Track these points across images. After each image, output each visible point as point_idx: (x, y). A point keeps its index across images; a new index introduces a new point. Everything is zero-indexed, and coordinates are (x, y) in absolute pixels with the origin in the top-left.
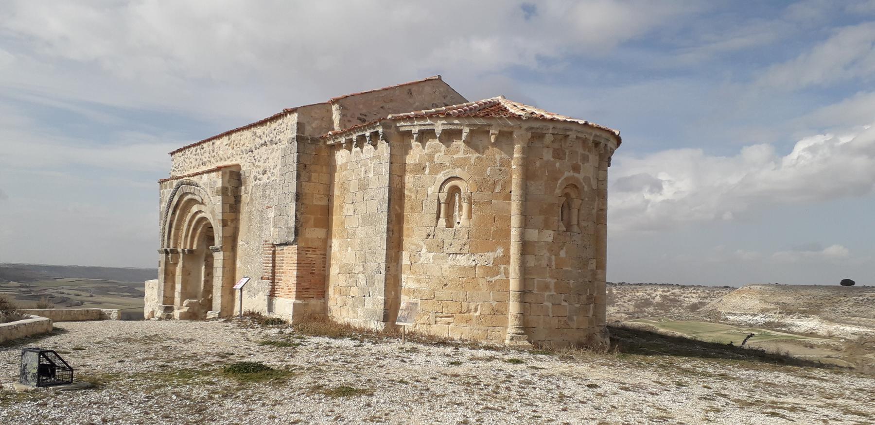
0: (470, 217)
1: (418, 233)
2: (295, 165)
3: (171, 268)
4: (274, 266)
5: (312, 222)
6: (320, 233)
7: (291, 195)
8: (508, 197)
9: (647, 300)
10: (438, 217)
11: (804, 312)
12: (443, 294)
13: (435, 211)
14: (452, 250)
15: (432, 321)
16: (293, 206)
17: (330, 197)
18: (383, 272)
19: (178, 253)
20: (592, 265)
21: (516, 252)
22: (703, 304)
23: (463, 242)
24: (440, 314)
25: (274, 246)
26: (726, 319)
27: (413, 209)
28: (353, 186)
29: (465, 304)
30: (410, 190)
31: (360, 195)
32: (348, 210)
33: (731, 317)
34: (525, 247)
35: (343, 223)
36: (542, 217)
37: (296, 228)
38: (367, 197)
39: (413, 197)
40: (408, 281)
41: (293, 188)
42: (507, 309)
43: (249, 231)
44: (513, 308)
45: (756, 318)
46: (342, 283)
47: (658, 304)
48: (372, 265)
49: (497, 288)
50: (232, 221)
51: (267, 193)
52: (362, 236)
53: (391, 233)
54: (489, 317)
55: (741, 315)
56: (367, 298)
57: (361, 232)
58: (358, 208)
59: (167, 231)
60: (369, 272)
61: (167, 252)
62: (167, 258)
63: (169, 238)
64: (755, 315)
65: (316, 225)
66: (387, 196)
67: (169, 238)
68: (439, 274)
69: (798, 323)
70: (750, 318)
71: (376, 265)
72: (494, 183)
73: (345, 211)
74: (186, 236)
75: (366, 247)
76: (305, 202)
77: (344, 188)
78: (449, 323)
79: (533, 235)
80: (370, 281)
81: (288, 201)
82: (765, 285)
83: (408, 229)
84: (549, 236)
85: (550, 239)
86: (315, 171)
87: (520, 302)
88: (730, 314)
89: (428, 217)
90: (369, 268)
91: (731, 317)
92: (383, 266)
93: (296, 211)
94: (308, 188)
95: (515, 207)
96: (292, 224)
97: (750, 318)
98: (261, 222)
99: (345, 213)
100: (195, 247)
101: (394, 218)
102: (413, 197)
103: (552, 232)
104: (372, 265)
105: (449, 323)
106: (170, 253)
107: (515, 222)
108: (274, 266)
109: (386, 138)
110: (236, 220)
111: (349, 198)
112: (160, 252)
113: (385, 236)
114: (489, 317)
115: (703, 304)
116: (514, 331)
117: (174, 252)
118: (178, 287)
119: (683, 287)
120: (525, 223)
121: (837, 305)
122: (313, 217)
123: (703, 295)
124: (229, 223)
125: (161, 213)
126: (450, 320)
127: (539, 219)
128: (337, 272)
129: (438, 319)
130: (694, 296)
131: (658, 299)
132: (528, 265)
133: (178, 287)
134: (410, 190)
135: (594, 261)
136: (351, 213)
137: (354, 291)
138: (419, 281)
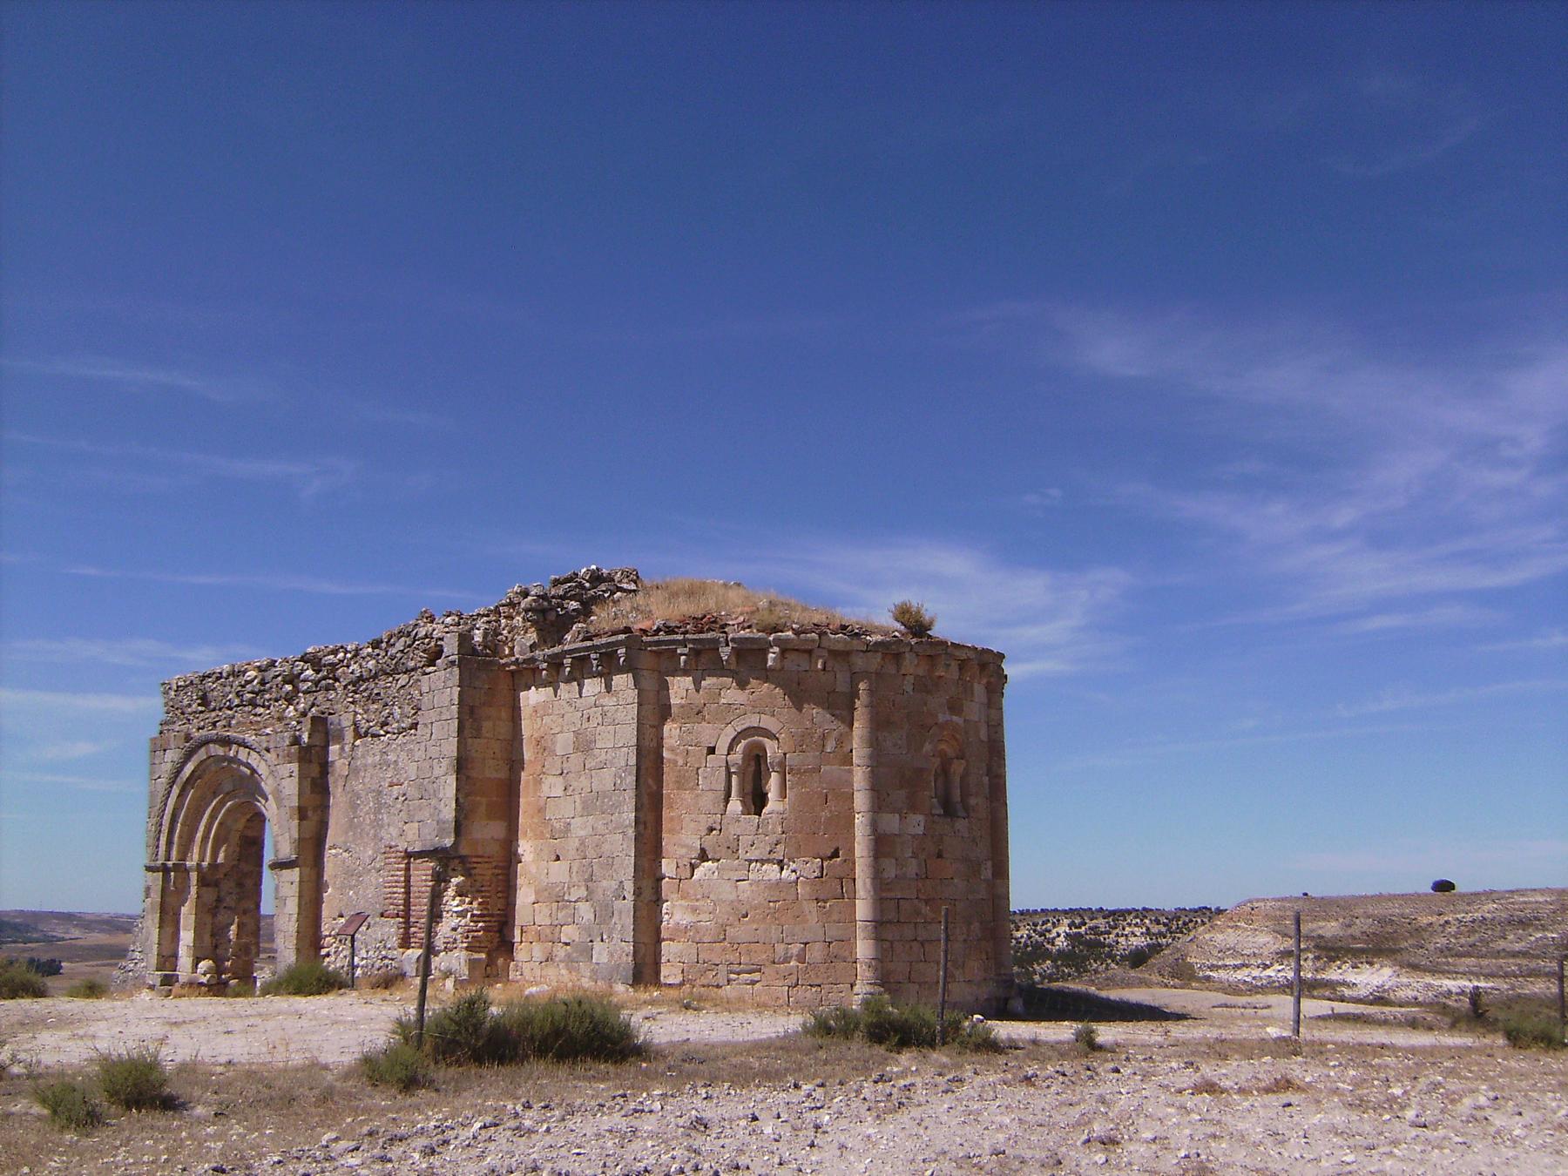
0: (783, 795)
1: (693, 825)
2: (455, 708)
3: (170, 900)
4: (408, 893)
5: (483, 809)
6: (496, 830)
7: (445, 763)
8: (847, 760)
9: (1038, 946)
10: (727, 800)
11: (1363, 951)
12: (738, 932)
13: (722, 786)
14: (754, 854)
15: (722, 981)
16: (452, 780)
17: (515, 764)
18: (630, 897)
19: (187, 871)
20: (987, 873)
21: (865, 853)
22: (1156, 949)
23: (773, 838)
24: (736, 968)
25: (409, 855)
26: (1208, 978)
27: (680, 785)
28: (563, 743)
29: (780, 948)
30: (672, 750)
31: (577, 759)
32: (553, 786)
33: (1221, 974)
34: (881, 845)
35: (541, 810)
36: (903, 793)
37: (457, 821)
38: (591, 763)
39: (680, 762)
40: (674, 913)
41: (451, 748)
42: (852, 950)
43: (351, 825)
44: (864, 949)
45: (1269, 972)
46: (543, 918)
47: (1061, 953)
48: (607, 885)
49: (835, 917)
50: (315, 810)
51: (392, 757)
52: (582, 833)
53: (641, 827)
54: (823, 968)
55: (1236, 967)
56: (597, 945)
57: (580, 828)
58: (575, 784)
59: (165, 829)
60: (599, 895)
61: (165, 870)
62: (166, 879)
63: (169, 843)
64: (1266, 967)
65: (491, 816)
66: (633, 761)
67: (191, 839)
68: (733, 897)
69: (1351, 976)
70: (1256, 973)
71: (614, 884)
72: (824, 737)
73: (545, 787)
74: (205, 838)
75: (591, 853)
76: (474, 774)
77: (542, 745)
78: (753, 983)
79: (891, 822)
80: (604, 914)
81: (438, 771)
82: (1283, 899)
83: (672, 819)
84: (916, 824)
85: (920, 830)
86: (489, 718)
87: (876, 939)
88: (1213, 967)
89: (709, 801)
90: (600, 891)
91: (1221, 974)
92: (629, 886)
93: (458, 790)
94: (475, 745)
95: (860, 778)
96: (449, 812)
97: (1256, 973)
98: (377, 811)
99: (545, 790)
100: (220, 860)
101: (645, 800)
102: (680, 762)
103: (921, 818)
104: (607, 885)
105: (753, 983)
106: (170, 875)
107: (861, 801)
108: (408, 893)
109: (630, 667)
110: (324, 808)
111: (553, 765)
112: (149, 869)
113: (631, 832)
114: (823, 968)
115: (1156, 949)
116: (868, 989)
117: (181, 869)
118: (187, 937)
119: (1113, 913)
120: (879, 804)
121: (1426, 935)
122: (484, 800)
123: (1155, 929)
124: (310, 813)
125: (152, 794)
126: (756, 976)
127: (899, 796)
128: (533, 898)
129: (733, 976)
130: (1138, 931)
131: (1061, 943)
132: (885, 875)
133: (187, 937)
134: (672, 750)
135: (989, 864)
136: (559, 792)
137: (568, 933)
138: (694, 910)
